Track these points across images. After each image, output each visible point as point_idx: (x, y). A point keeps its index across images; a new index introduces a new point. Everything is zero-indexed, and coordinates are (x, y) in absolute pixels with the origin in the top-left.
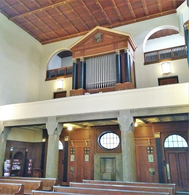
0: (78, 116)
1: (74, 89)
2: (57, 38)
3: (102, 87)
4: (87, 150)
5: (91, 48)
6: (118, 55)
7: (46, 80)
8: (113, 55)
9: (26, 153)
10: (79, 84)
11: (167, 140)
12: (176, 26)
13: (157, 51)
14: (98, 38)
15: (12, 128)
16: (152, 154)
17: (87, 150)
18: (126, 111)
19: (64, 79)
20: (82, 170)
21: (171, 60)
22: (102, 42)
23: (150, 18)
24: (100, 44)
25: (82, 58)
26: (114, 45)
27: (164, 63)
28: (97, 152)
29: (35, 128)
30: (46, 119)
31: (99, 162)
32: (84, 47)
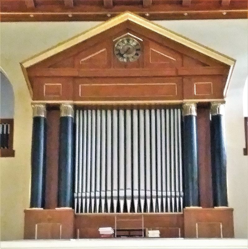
1: (37, 206)
3: (132, 209)
8: (165, 113)
14: (128, 51)
22: (140, 64)
23: (37, 19)
24: (135, 72)
25: (67, 105)
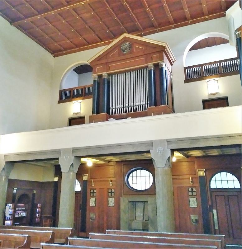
0: (99, 148)
1: (94, 114)
2: (73, 48)
3: (131, 111)
4: (111, 191)
5: (117, 61)
6: (151, 70)
7: (59, 102)
8: (145, 70)
9: (34, 195)
10: (101, 107)
11: (213, 179)
12: (225, 34)
13: (202, 65)
14: (126, 49)
15: (15, 164)
16: (195, 197)
17: (111, 191)
18: (161, 141)
19: (82, 100)
20: (105, 217)
21: (219, 77)
22: (130, 53)
23: (192, 23)
24: (129, 56)
25: (105, 74)
26: (146, 58)
27: (209, 81)
28: (124, 195)
29: (45, 163)
30: (59, 151)
31: (127, 207)
32: (108, 60)
